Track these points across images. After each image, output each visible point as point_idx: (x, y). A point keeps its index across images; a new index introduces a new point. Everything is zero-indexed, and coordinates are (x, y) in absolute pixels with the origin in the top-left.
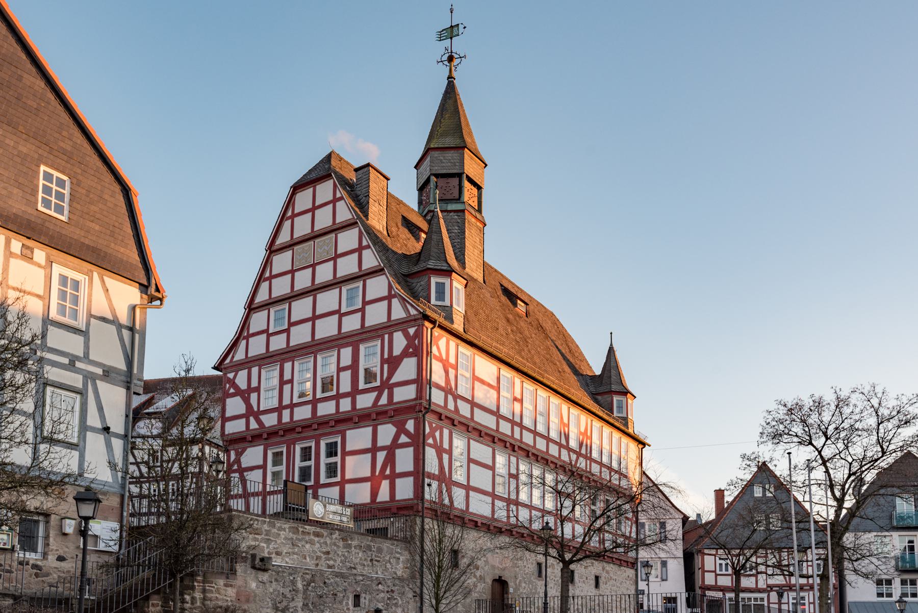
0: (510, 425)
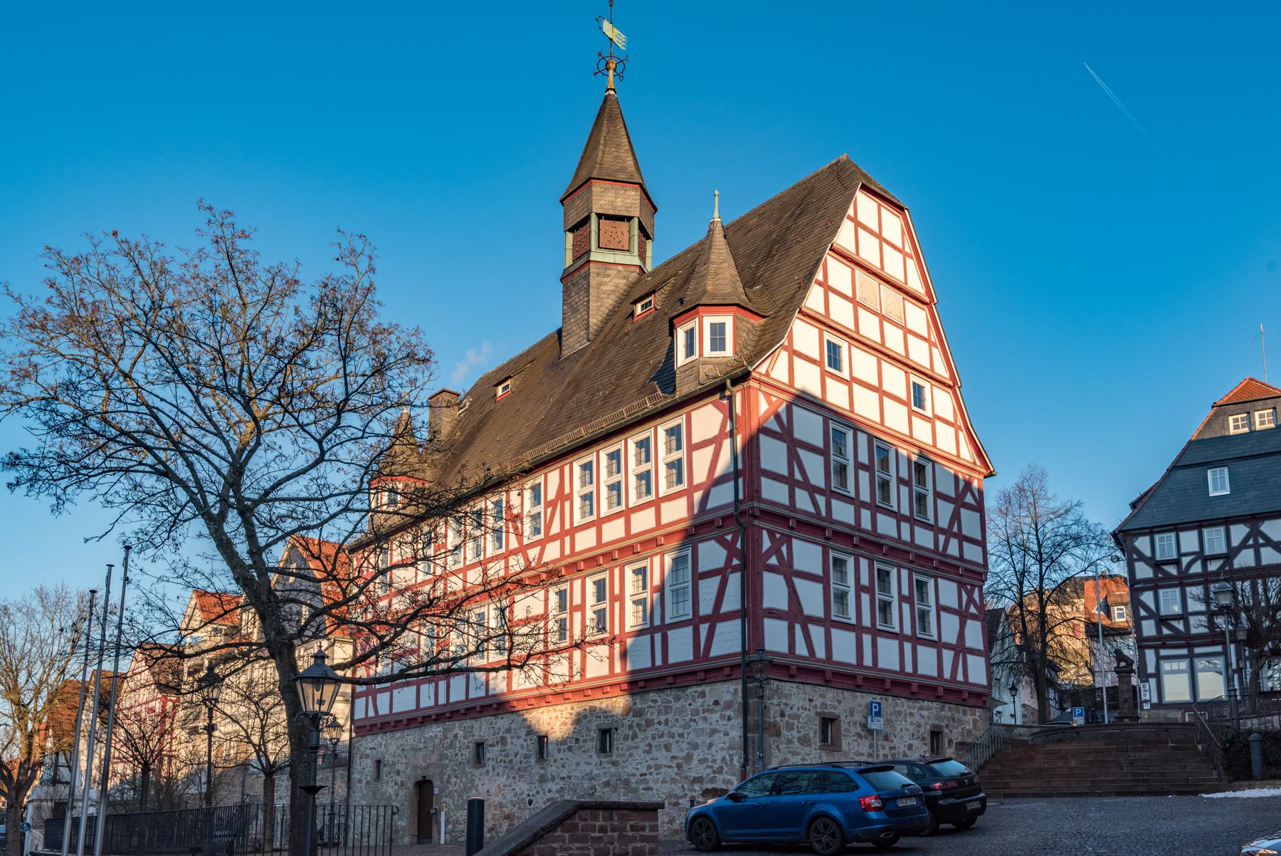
0: (852, 508)
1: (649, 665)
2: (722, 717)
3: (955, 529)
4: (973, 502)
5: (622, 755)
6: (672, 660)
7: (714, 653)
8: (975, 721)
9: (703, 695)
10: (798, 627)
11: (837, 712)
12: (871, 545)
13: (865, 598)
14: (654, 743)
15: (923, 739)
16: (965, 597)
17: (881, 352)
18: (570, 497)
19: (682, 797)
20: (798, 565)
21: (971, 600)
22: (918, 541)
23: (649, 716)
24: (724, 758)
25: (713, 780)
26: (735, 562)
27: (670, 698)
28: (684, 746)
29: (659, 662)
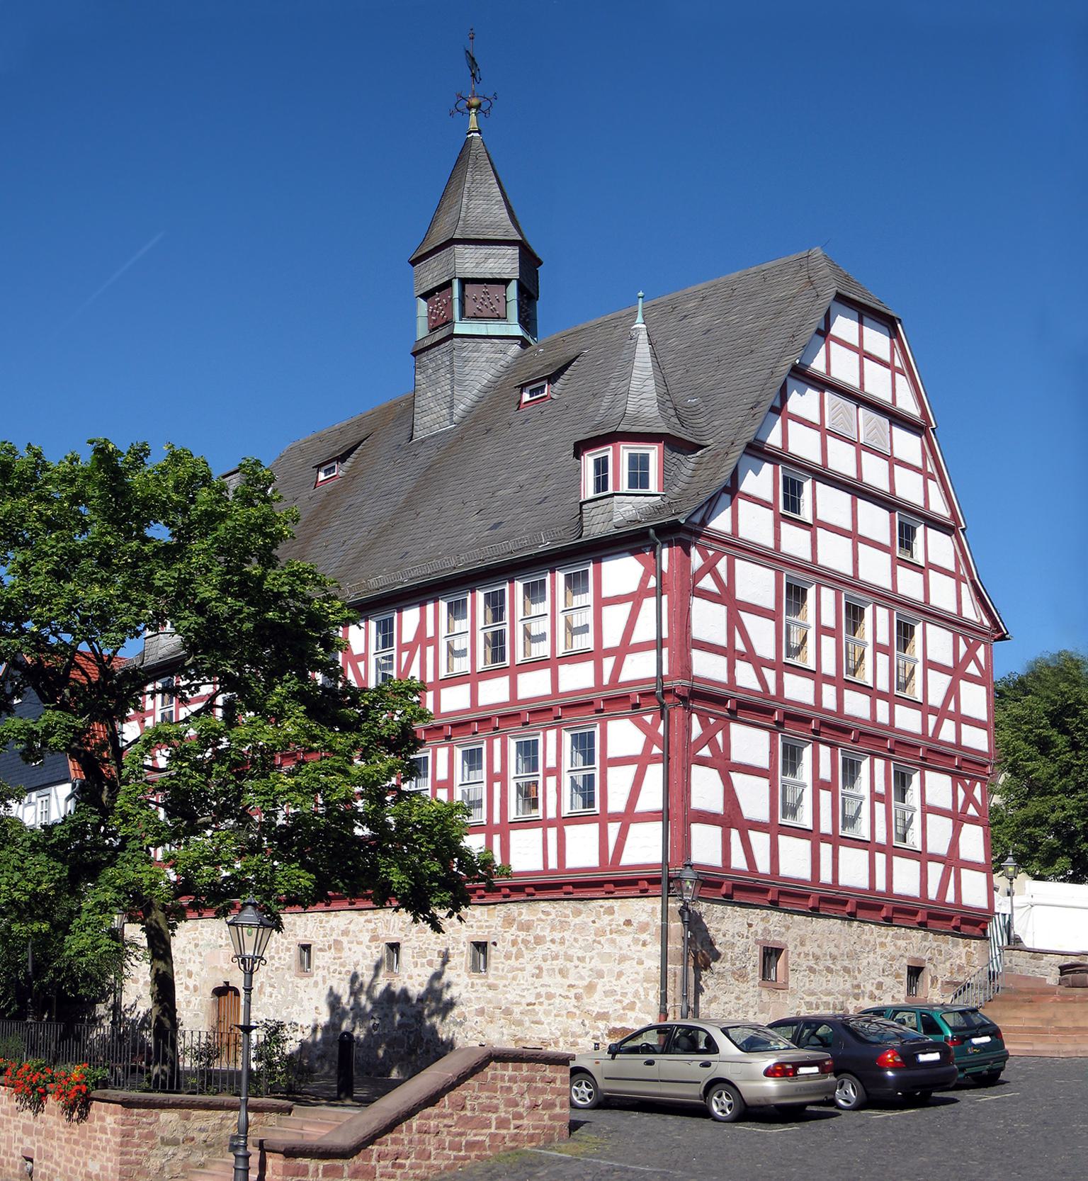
1: (540, 867)
2: (636, 941)
3: (952, 707)
4: (977, 673)
5: (502, 978)
6: (570, 864)
7: (626, 860)
8: (969, 954)
9: (610, 911)
10: (735, 834)
11: (783, 940)
12: (834, 729)
13: (825, 796)
14: (545, 966)
15: (898, 976)
16: (961, 794)
17: (857, 490)
18: (434, 641)
19: (580, 1036)
20: (736, 757)
21: (970, 799)
22: (899, 724)
23: (539, 932)
24: (637, 992)
25: (621, 1018)
26: (656, 750)
27: (568, 912)
28: (585, 973)
29: (553, 864)
